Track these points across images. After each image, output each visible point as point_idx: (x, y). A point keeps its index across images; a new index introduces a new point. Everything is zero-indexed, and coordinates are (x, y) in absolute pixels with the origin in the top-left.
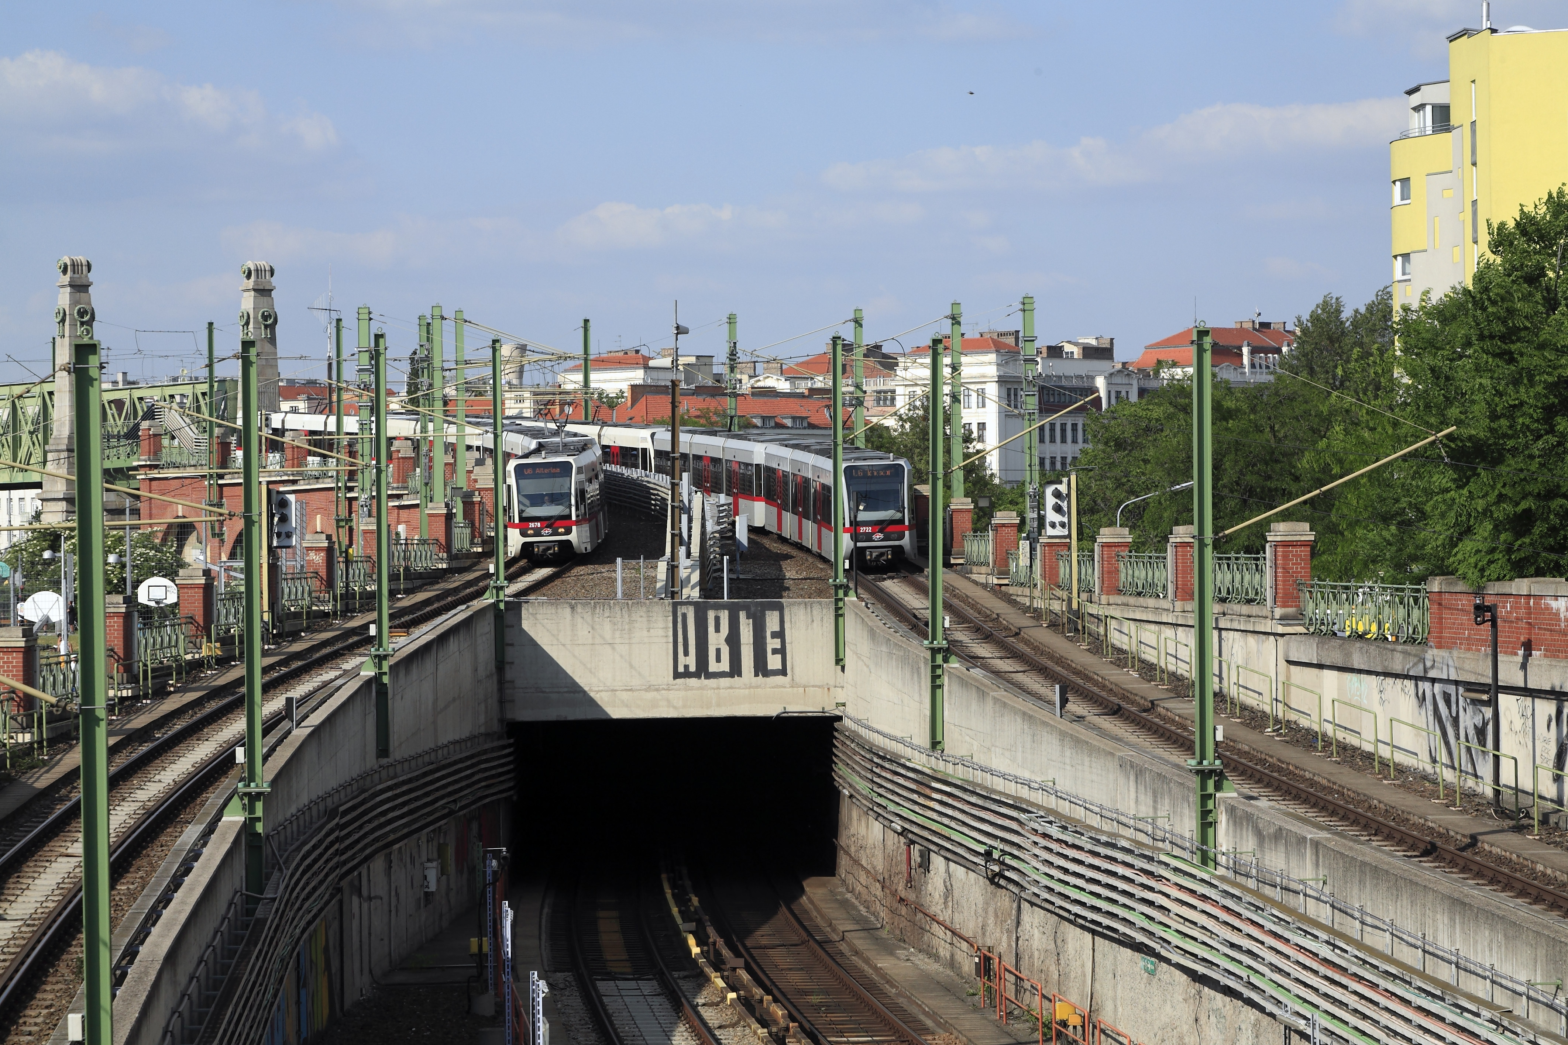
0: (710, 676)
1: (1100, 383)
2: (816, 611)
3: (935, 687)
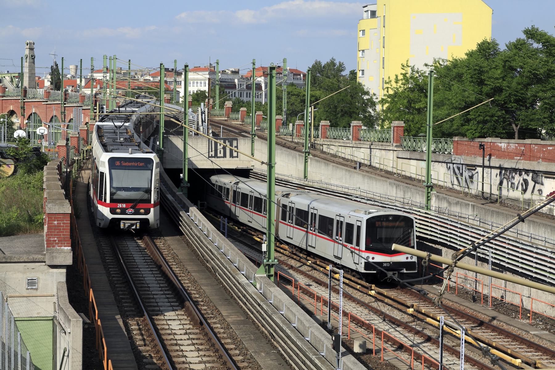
0: (218, 157)
1: (236, 81)
2: (246, 141)
3: (306, 162)
